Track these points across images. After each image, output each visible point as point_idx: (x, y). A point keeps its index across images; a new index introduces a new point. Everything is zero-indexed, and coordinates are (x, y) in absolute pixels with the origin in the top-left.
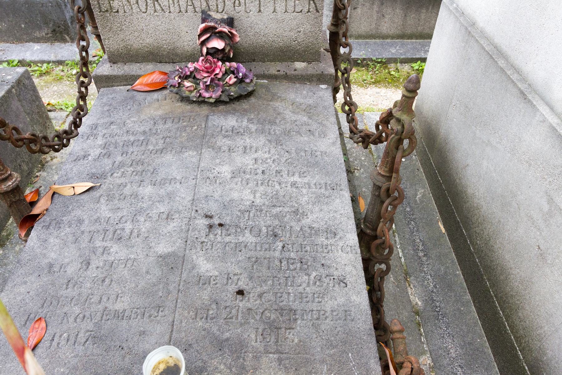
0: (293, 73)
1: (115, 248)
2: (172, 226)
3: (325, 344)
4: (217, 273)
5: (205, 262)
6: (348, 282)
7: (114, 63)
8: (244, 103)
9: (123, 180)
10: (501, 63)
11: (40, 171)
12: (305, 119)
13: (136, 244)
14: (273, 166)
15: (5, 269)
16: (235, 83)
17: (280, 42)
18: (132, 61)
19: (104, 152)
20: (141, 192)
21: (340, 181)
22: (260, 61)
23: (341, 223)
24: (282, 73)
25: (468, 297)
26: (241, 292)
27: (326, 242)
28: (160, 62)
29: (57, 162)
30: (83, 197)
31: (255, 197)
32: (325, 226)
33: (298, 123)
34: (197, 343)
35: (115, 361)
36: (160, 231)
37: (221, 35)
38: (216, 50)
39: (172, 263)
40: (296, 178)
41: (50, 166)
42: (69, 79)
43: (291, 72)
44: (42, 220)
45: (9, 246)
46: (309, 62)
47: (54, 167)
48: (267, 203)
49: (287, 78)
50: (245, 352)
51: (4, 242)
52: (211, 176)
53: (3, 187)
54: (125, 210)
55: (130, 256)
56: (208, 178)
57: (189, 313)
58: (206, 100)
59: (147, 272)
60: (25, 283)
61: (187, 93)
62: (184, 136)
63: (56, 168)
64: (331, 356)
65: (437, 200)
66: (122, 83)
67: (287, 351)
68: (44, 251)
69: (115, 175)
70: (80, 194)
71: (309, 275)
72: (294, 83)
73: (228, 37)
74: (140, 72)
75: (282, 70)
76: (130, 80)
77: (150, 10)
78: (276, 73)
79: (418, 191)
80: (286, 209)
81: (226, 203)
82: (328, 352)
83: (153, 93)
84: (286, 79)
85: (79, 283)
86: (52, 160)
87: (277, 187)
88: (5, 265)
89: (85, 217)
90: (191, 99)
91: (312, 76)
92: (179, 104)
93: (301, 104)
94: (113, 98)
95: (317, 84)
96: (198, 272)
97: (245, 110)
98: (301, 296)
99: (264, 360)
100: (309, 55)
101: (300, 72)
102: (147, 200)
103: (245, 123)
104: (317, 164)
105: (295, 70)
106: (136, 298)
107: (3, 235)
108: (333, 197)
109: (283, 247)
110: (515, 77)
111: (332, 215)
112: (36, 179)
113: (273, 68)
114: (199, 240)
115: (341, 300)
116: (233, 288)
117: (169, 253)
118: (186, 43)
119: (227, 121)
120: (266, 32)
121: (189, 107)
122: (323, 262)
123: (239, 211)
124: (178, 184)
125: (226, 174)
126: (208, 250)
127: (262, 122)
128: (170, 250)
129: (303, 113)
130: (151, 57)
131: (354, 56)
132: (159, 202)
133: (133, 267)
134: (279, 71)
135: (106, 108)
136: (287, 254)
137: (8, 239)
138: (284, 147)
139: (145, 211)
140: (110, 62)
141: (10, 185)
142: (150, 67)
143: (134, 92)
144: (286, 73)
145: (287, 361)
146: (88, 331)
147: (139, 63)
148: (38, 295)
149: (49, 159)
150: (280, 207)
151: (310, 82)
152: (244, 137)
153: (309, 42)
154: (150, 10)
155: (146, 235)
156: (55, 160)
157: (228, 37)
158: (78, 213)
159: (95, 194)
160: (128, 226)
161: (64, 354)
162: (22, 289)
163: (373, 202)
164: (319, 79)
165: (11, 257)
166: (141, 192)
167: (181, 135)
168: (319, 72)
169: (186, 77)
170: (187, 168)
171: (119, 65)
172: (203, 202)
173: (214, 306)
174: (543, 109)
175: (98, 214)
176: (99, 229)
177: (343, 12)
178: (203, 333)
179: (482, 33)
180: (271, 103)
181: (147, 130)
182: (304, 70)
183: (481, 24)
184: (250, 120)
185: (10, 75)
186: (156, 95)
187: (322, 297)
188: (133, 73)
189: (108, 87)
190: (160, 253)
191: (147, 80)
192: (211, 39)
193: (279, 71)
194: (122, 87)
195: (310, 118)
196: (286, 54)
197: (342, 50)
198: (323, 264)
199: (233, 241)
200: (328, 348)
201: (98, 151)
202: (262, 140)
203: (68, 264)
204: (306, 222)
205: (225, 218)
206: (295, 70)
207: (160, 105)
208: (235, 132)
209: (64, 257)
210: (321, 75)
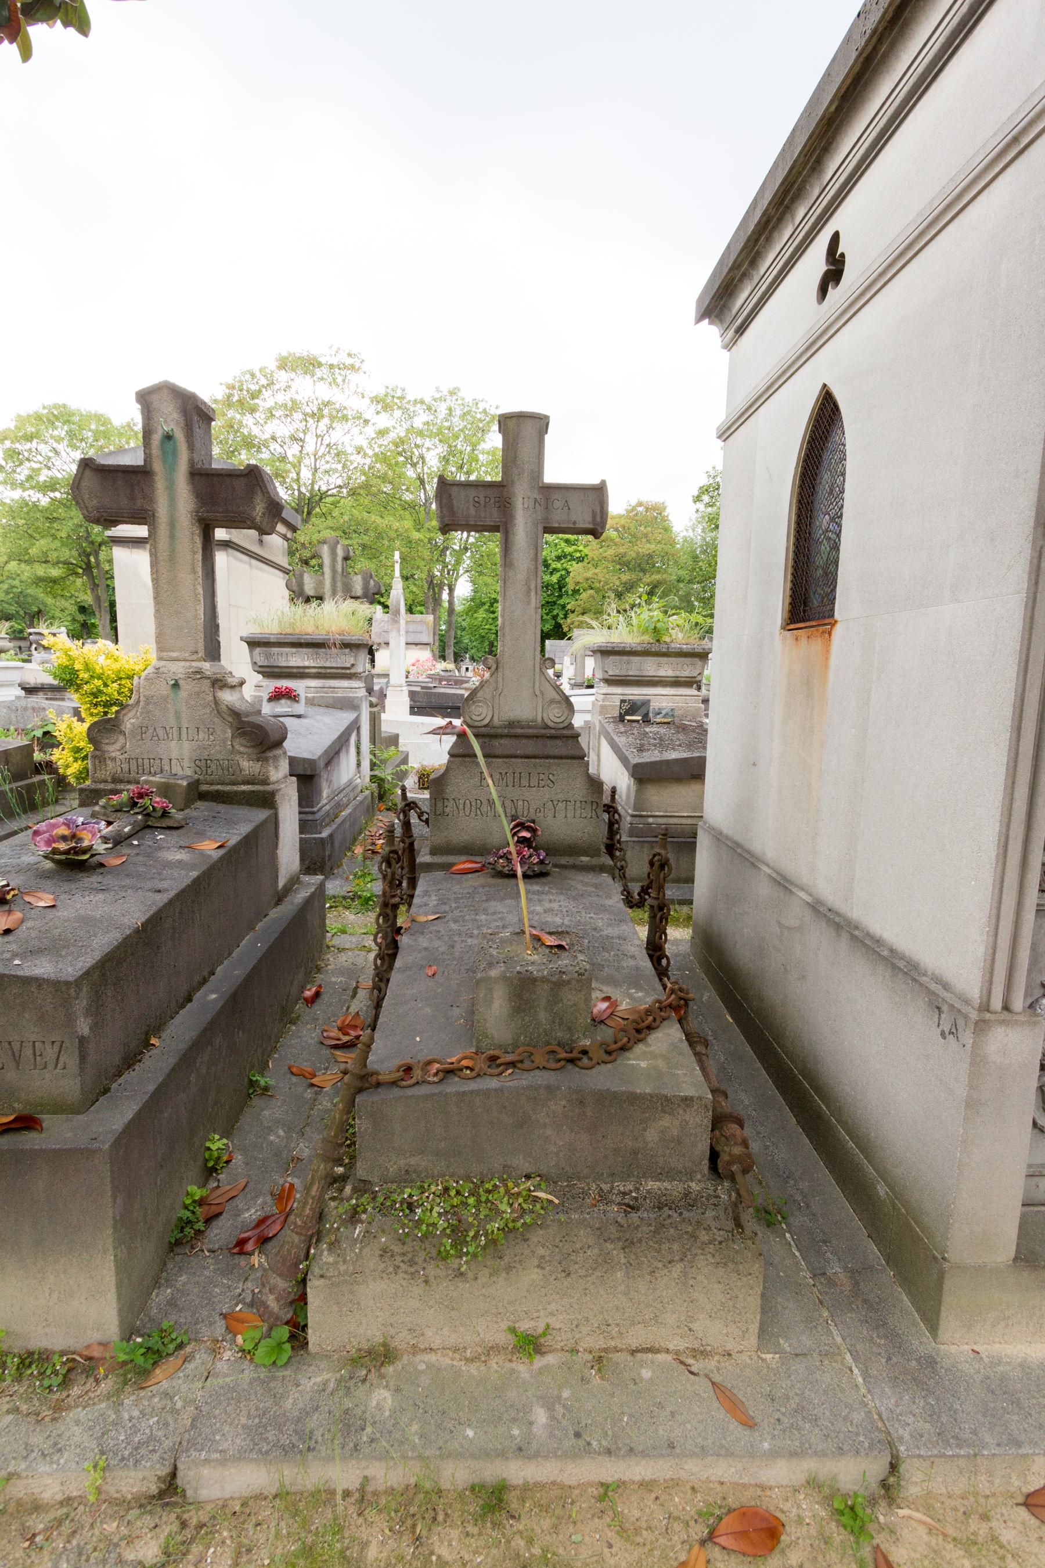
10: (739, 850)
25: (759, 1065)
37: (528, 829)
43: (578, 863)
49: (574, 867)
61: (500, 868)
65: (722, 996)
73: (533, 831)
74: (455, 861)
77: (473, 814)
79: (879, 1554)
100: (590, 850)
110: (748, 856)
113: (564, 860)
126: (688, 578)
142: (463, 858)
154: (473, 814)
157: (533, 831)
169: (501, 857)
174: (765, 868)
177: (616, 826)
179: (727, 837)
183: (725, 832)
196: (573, 850)
197: (618, 853)
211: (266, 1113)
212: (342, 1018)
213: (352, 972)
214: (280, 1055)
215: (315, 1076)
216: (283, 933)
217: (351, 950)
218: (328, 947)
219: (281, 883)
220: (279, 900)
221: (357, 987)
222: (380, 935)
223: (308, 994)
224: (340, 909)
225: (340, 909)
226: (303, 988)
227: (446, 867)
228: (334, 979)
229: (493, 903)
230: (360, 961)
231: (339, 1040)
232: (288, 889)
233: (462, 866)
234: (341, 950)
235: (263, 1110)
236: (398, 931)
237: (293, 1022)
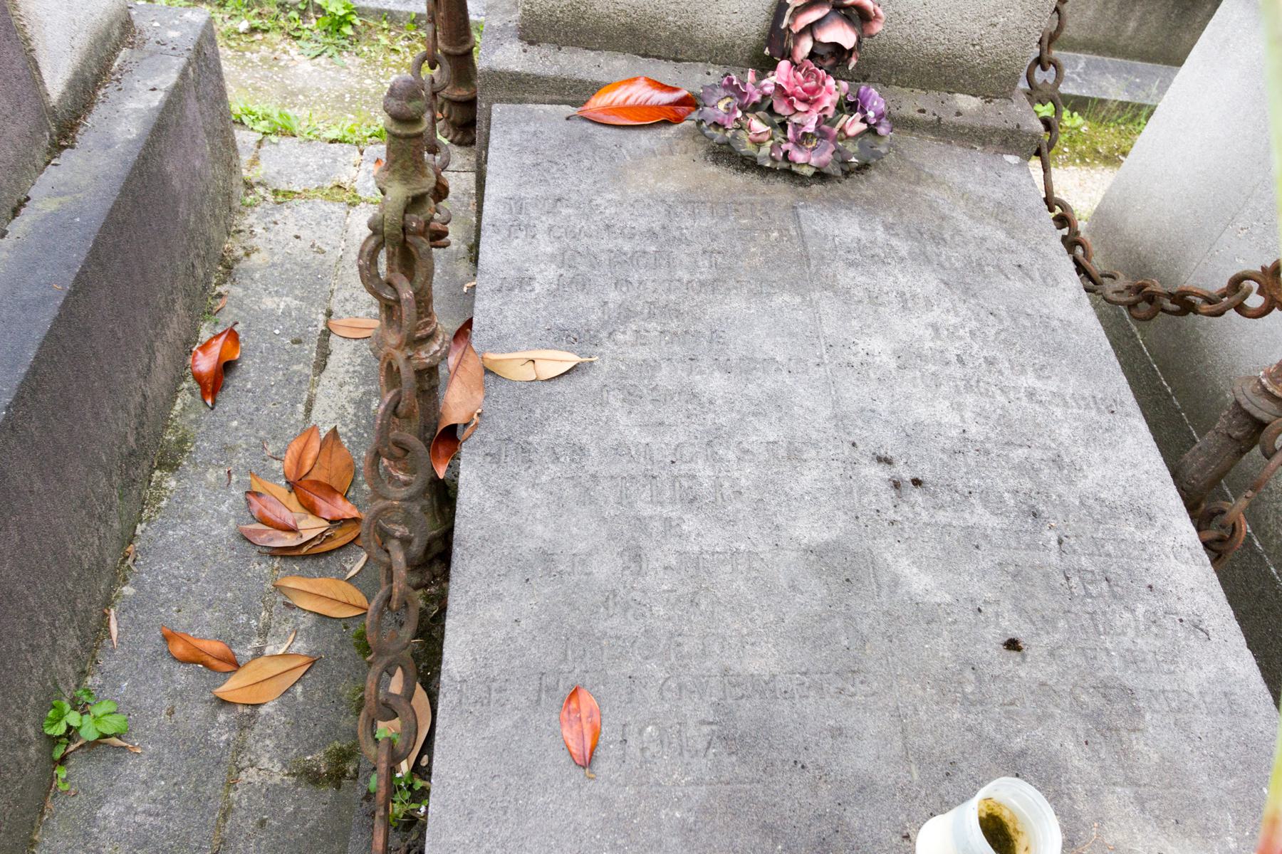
0: (954, 119)
1: (690, 524)
2: (809, 478)
3: (1211, 765)
4: (948, 598)
5: (915, 570)
6: (1210, 629)
7: (531, 43)
8: (862, 182)
9: (641, 353)
11: (225, 282)
12: (1001, 235)
13: (740, 516)
14: (976, 347)
15: (193, 527)
16: (861, 134)
17: (940, 44)
18: (577, 44)
19: (568, 274)
20: (701, 386)
21: (1119, 392)
22: (880, 81)
23: (1152, 492)
24: (929, 117)
26: (1012, 645)
27: (1138, 536)
28: (645, 55)
29: (260, 262)
30: (560, 386)
31: (963, 420)
32: (1126, 498)
33: (989, 244)
34: (966, 759)
35: (797, 795)
36: (787, 489)
38: (837, 48)
39: (843, 567)
40: (1029, 380)
41: (246, 271)
42: (233, 44)
44: (476, 438)
45: (190, 469)
46: (988, 99)
47: (257, 276)
48: (992, 435)
49: (938, 129)
50: (1068, 782)
51: (174, 457)
52: (855, 361)
53: (423, 354)
54: (680, 429)
55: (737, 545)
56: (850, 365)
57: (924, 689)
58: (794, 168)
59: (793, 588)
60: (498, 597)
62: (754, 254)
63: (263, 276)
64: (1231, 792)
66: (548, 97)
67: (1147, 780)
68: (515, 520)
69: (620, 337)
70: (549, 380)
71: (1133, 611)
72: (950, 143)
75: (930, 110)
76: (574, 92)
78: (918, 115)
80: (1037, 454)
81: (910, 432)
82: (1223, 784)
83: (635, 133)
84: (933, 133)
85: (632, 603)
86: (247, 255)
87: (1001, 399)
88: (190, 516)
89: (585, 439)
90: (760, 162)
91: (994, 132)
92: (713, 169)
93: (981, 198)
94: (535, 134)
95: (996, 153)
96: (908, 593)
97: (869, 202)
98: (1132, 659)
99: (1110, 800)
100: (990, 81)
101: (969, 121)
102: (725, 408)
103: (880, 233)
104: (1059, 350)
105: (959, 114)
106: (789, 648)
107: (169, 441)
108: (1119, 431)
109: (1060, 542)
111: (1130, 474)
112: (220, 303)
113: (912, 103)
114: (884, 516)
115: (1210, 670)
116: (993, 637)
117: (827, 544)
118: (724, 17)
119: (837, 225)
120: (921, 15)
121: (740, 180)
122: (1149, 582)
123: (943, 450)
124: (785, 373)
125: (885, 358)
127: (916, 234)
128: (826, 536)
129: (992, 221)
130: (627, 38)
131: (1066, 89)
132: (754, 414)
133: (754, 574)
134: (922, 111)
135: (529, 160)
136: (1072, 560)
137: (183, 451)
138: (982, 301)
139: (730, 435)
140: (521, 38)
141: (436, 352)
142: (620, 64)
143: (586, 125)
144: (939, 119)
145: (1155, 804)
146: (703, 722)
147: (592, 50)
148: (543, 629)
149: (240, 253)
150: (1021, 446)
151: (983, 144)
152: (889, 268)
153: (1006, 53)
155: (755, 496)
156: (254, 257)
158: (561, 426)
159: (589, 382)
160: (704, 471)
161: (667, 775)
162: (497, 612)
163: (1215, 450)
164: (1006, 140)
165: (201, 498)
166: (701, 386)
167: (745, 250)
168: (1010, 125)
170: (791, 334)
171: (545, 49)
172: (859, 423)
173: (969, 675)
175: (616, 435)
176: (633, 472)
178: (969, 736)
180: (919, 189)
181: (656, 227)
182: (978, 115)
184: (888, 228)
185: (174, 27)
186: (645, 139)
187: (1173, 662)
188: (582, 75)
189: (510, 101)
190: (805, 541)
191: (622, 98)
192: (828, 21)
193: (922, 111)
194: (548, 107)
195: (1009, 234)
196: (942, 73)
198: (1150, 587)
199: (954, 523)
200: (1221, 776)
201: (552, 272)
202: (928, 283)
203: (590, 554)
204: (200, 354)
205: (920, 466)
206: (959, 114)
207: (663, 170)
208: (864, 257)
209: (572, 536)
210: (1013, 132)
211: (109, 810)
212: (296, 447)
213: (310, 279)
214: (138, 585)
215: (235, 665)
216: (81, 286)
217: (304, 195)
218: (249, 186)
219: (56, 82)
220: (64, 129)
221: (327, 333)
222: (383, 258)
223: (205, 364)
224: (275, 37)
225: (275, 37)
226: (188, 344)
227: (574, 92)
228: (269, 303)
229: (736, 305)
230: (329, 237)
231: (292, 530)
232: (92, 82)
233: (618, 96)
234: (283, 197)
235: (100, 801)
236: (449, 438)
237: (170, 464)
